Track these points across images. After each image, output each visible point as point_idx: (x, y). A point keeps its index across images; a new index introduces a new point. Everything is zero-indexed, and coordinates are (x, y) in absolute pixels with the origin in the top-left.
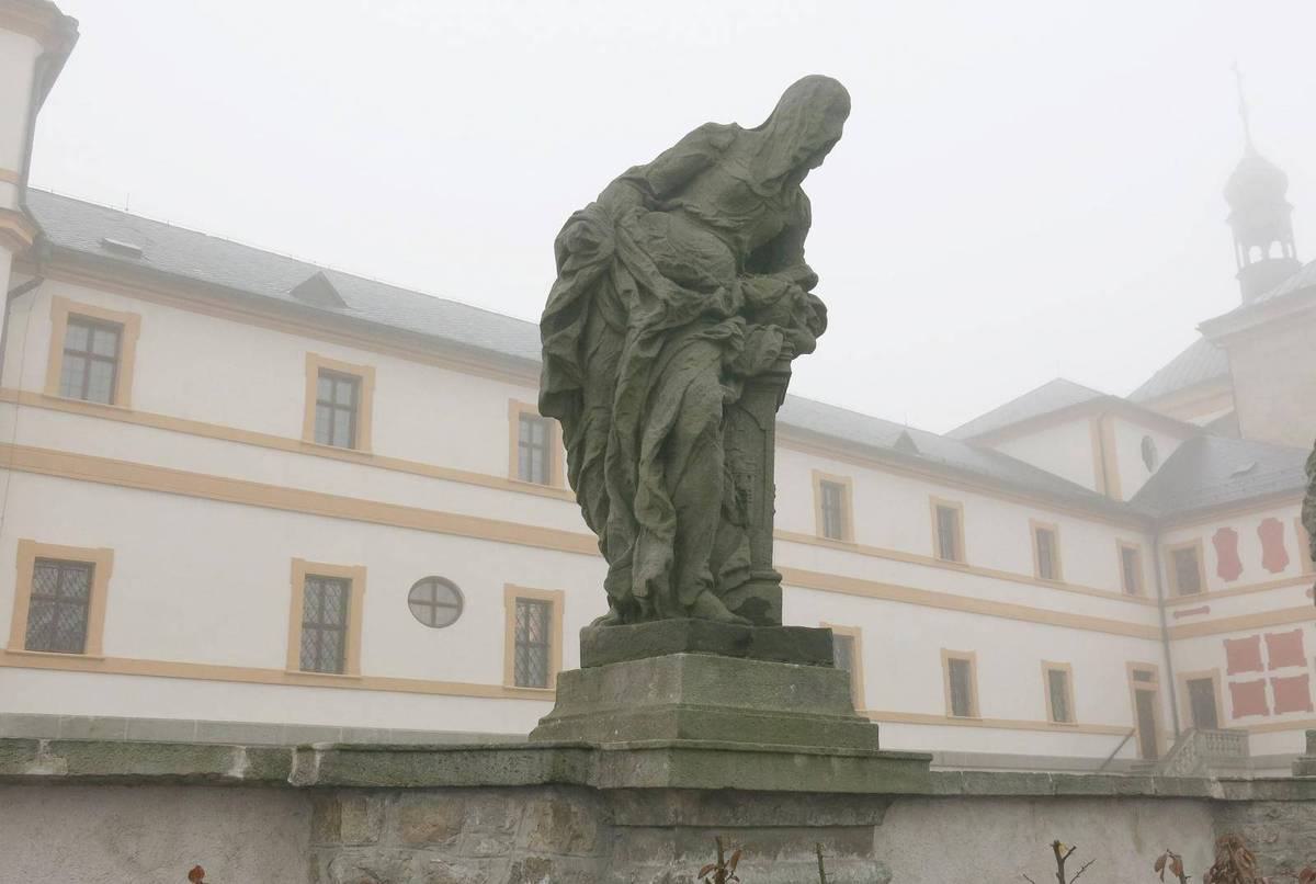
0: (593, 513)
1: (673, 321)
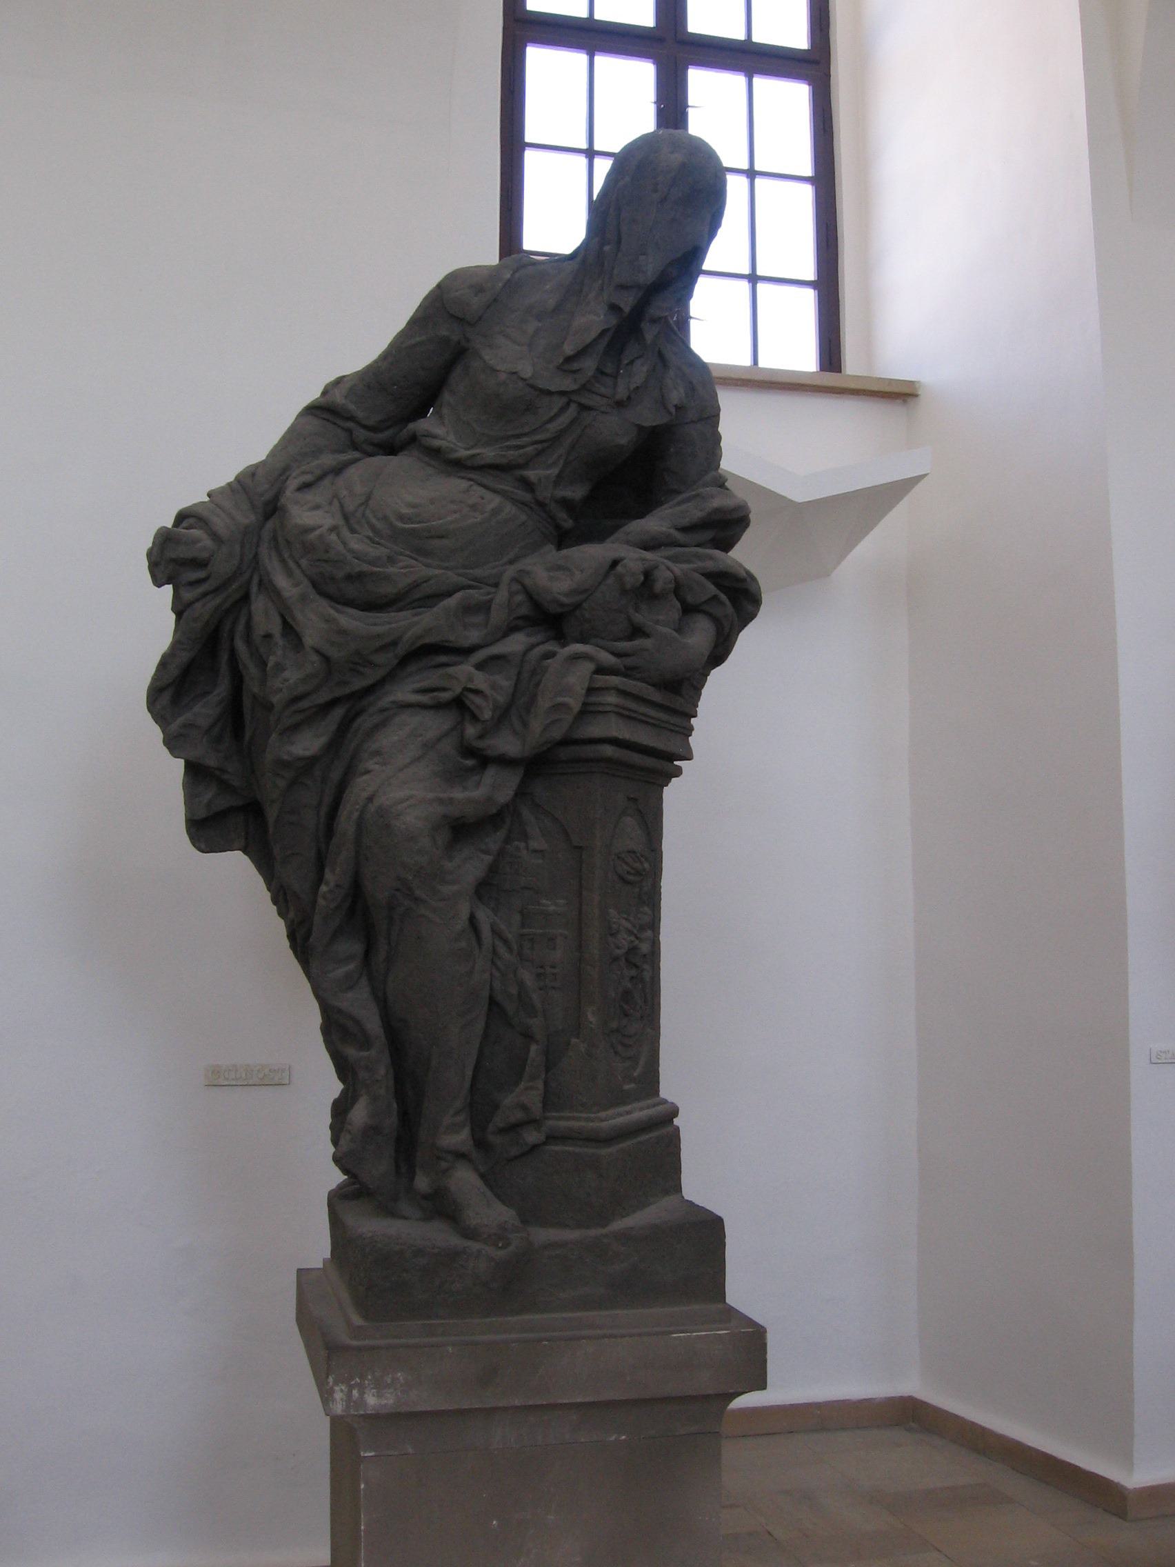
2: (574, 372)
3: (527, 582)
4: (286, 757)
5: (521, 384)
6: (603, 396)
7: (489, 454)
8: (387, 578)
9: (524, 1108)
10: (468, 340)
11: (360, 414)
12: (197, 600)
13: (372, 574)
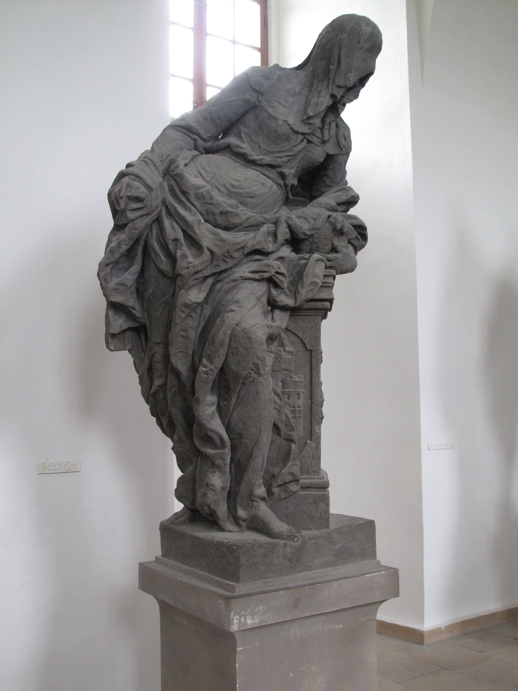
0: (165, 426)
1: (218, 266)
2: (310, 124)
3: (290, 222)
4: (188, 302)
5: (287, 127)
6: (318, 137)
7: (268, 159)
8: (237, 215)
9: (292, 474)
10: (259, 102)
11: (201, 132)
12: (137, 219)
13: (232, 212)
